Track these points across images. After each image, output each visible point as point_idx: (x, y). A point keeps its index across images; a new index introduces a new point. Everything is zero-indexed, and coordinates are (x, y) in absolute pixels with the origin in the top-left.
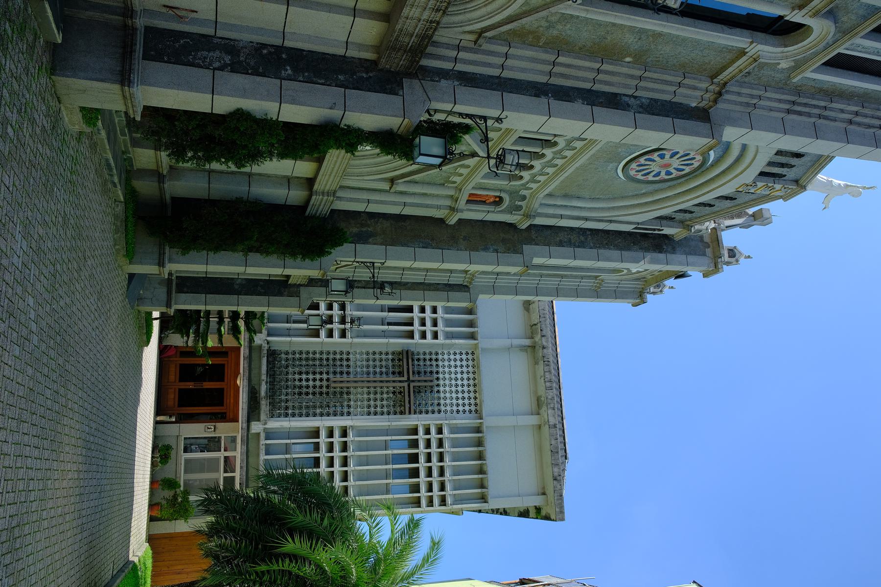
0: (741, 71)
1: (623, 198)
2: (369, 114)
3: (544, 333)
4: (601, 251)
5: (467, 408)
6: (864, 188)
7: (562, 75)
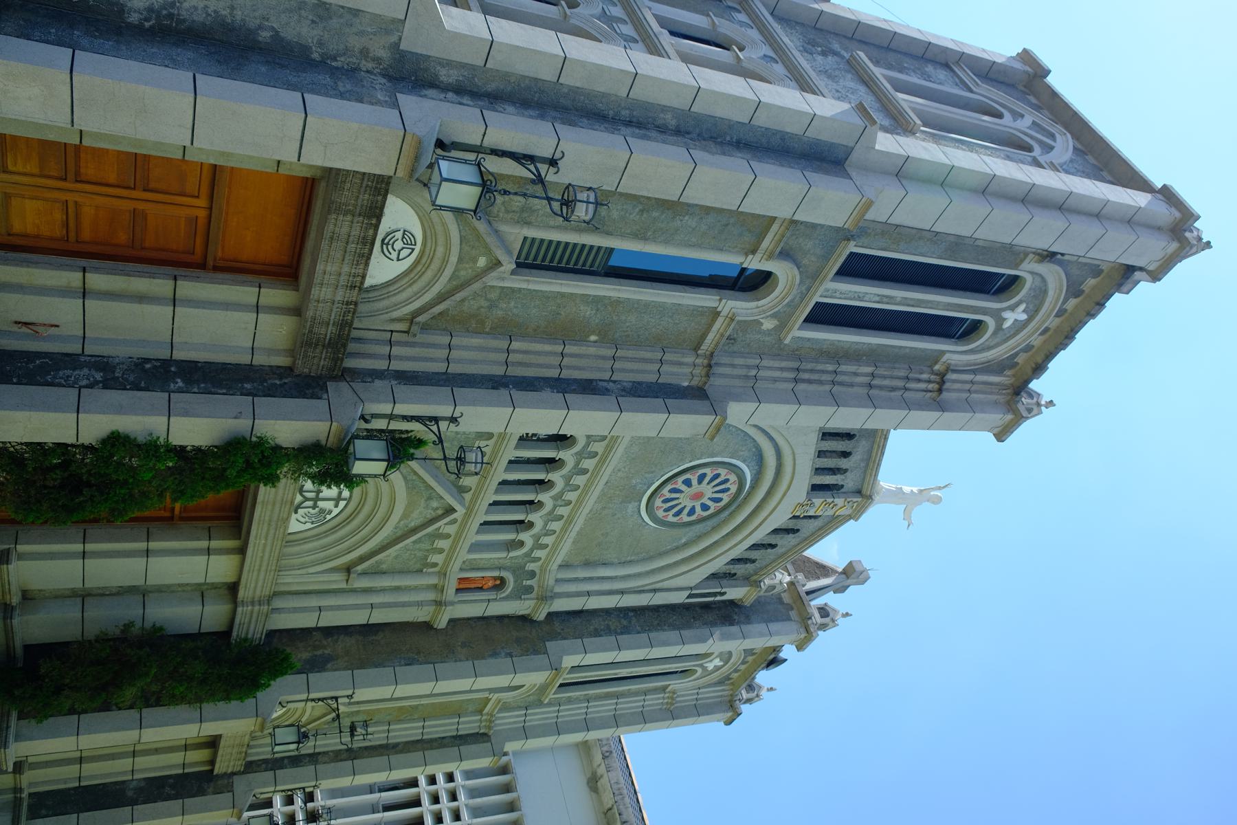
0: (722, 335)
1: (662, 554)
2: (288, 426)
3: (625, 817)
4: (653, 635)
6: (940, 488)
7: (520, 364)
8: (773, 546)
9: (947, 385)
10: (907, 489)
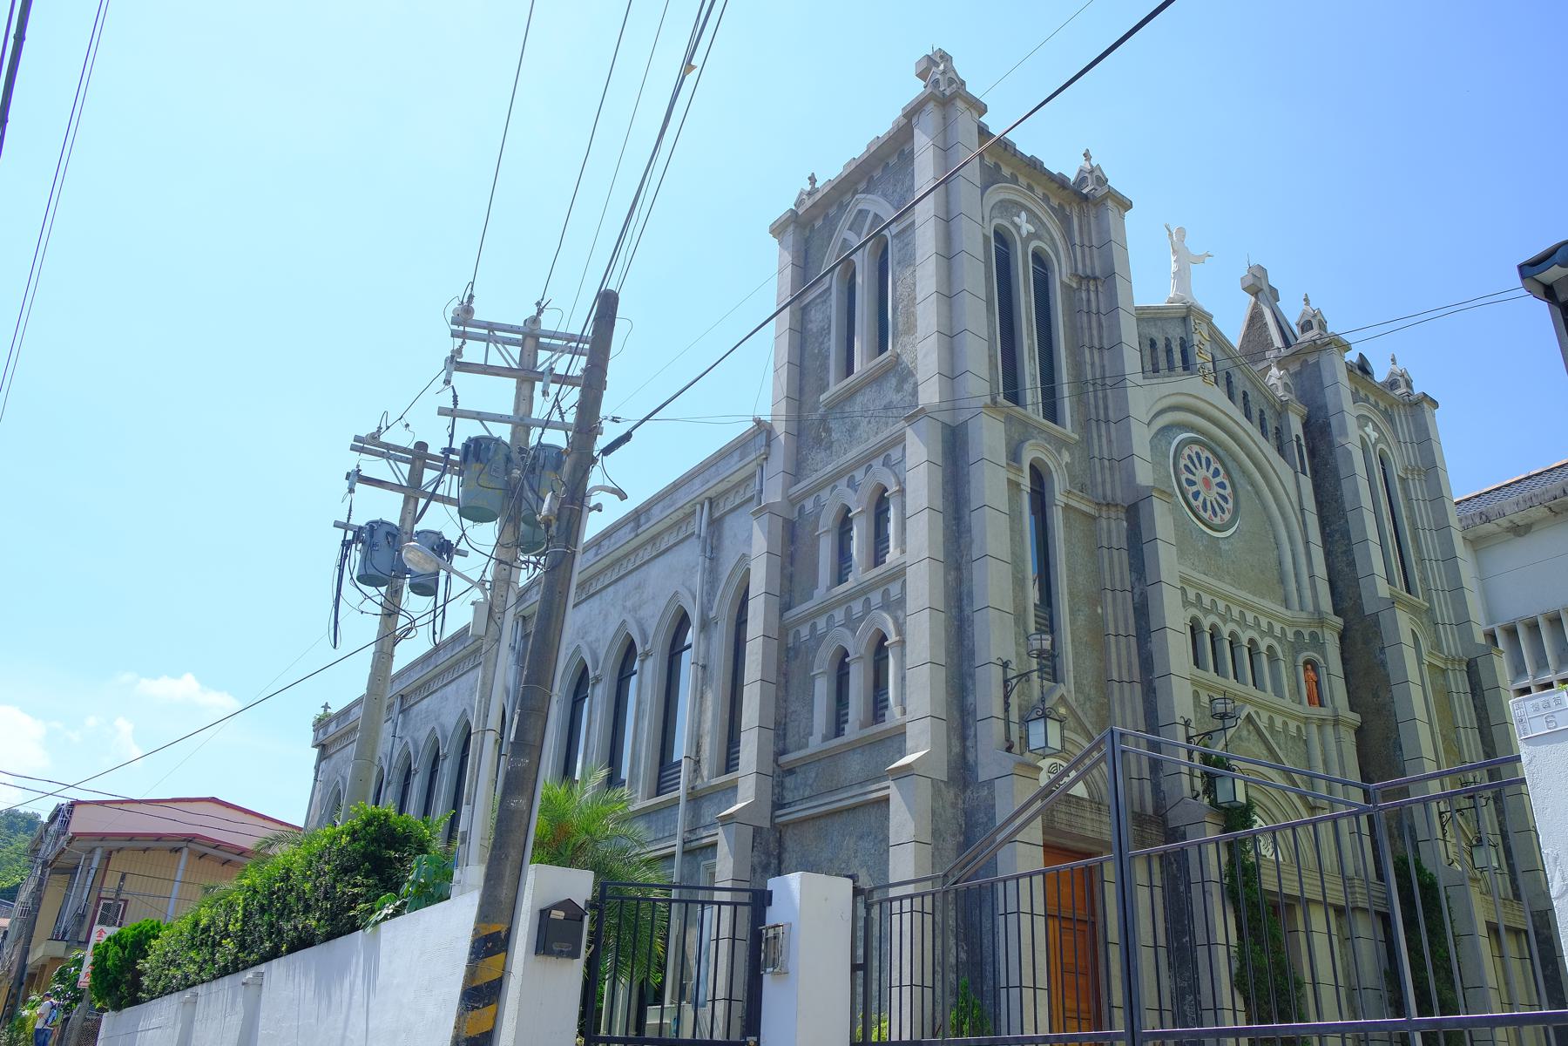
1: (1265, 508)
4: (1348, 506)
6: (1171, 235)
7: (1130, 670)
8: (1245, 394)
9: (1089, 272)
10: (1174, 267)
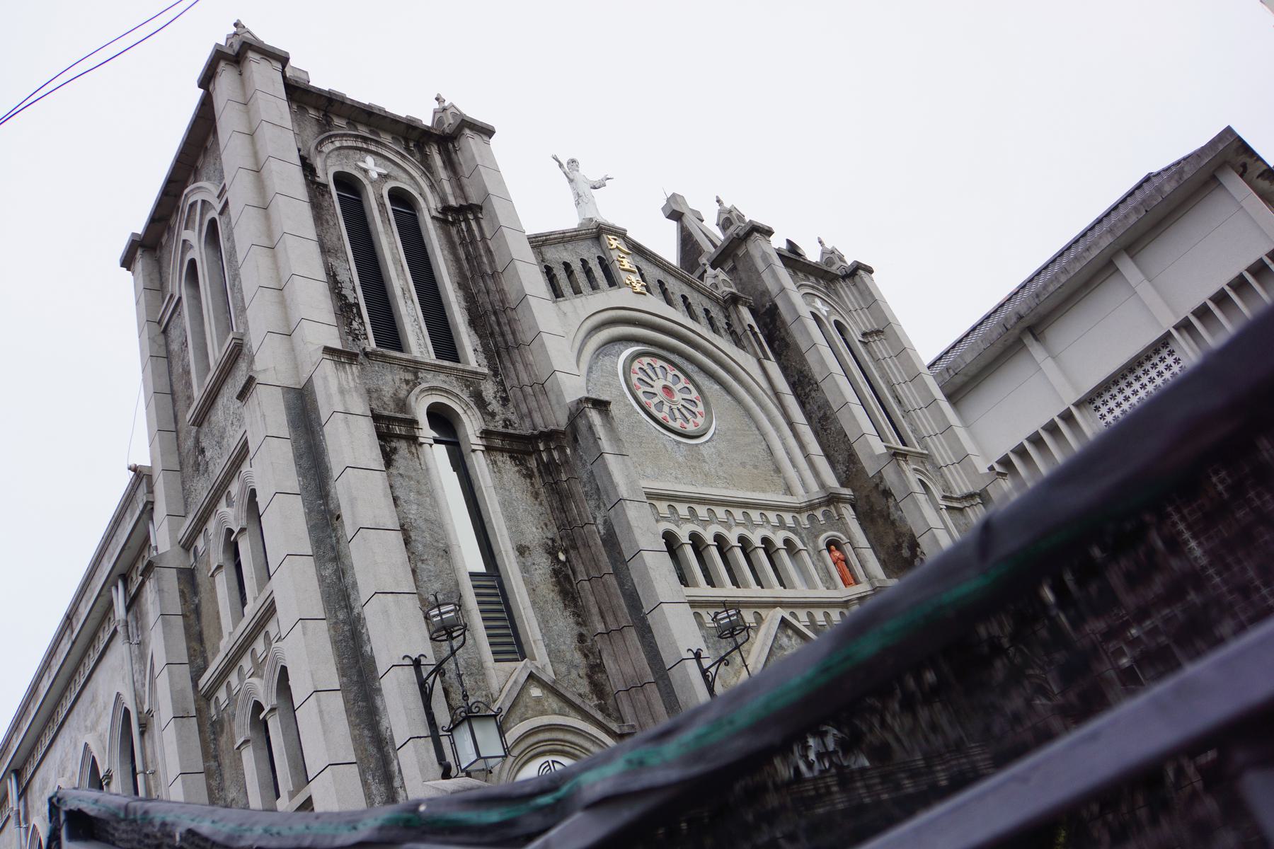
5: (1170, 360)
